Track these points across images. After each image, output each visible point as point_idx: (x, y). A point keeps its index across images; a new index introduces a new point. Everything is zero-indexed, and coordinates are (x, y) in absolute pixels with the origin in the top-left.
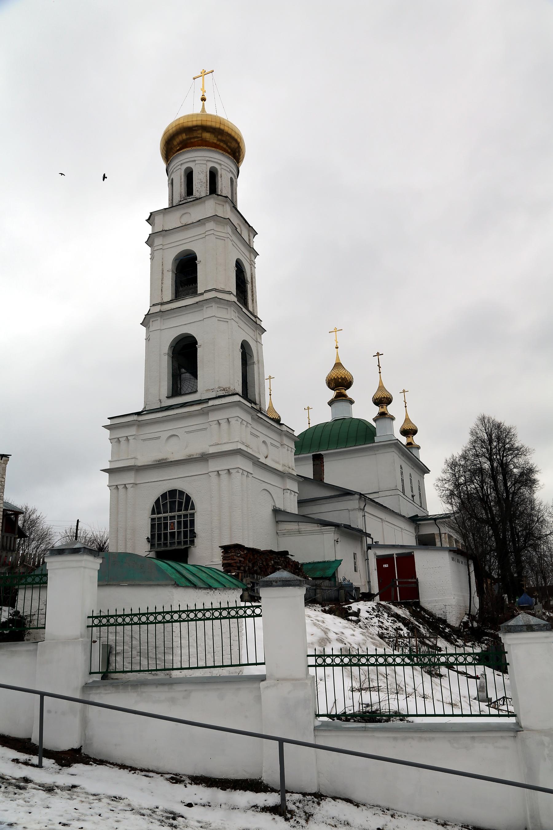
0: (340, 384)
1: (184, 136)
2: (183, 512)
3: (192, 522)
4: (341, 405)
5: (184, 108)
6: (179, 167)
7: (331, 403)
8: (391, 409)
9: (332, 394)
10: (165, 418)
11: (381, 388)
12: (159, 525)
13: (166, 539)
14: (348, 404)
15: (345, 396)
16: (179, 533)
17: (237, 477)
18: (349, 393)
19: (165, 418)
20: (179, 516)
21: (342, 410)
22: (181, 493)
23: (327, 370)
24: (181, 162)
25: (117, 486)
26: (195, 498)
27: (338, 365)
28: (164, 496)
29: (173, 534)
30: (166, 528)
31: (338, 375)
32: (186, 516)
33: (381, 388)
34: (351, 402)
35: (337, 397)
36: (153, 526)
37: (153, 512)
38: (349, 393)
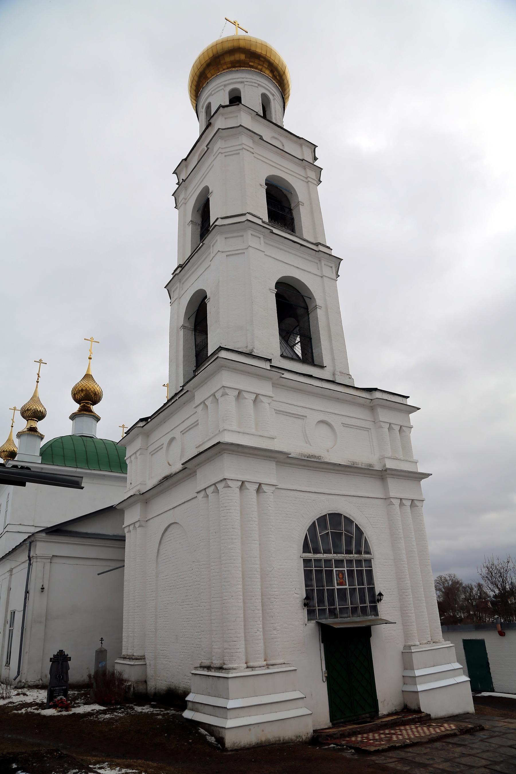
0: (87, 399)
1: (243, 57)
2: (354, 556)
3: (370, 573)
4: (86, 420)
5: (215, 33)
6: (223, 87)
7: (73, 417)
8: (40, 426)
9: (76, 407)
10: (319, 390)
11: (35, 398)
12: (319, 572)
13: (332, 602)
14: (94, 422)
15: (91, 411)
16: (353, 591)
17: (232, 495)
18: (95, 409)
19: (319, 390)
20: (350, 562)
21: (85, 426)
22: (349, 521)
23: (76, 379)
24: (260, 83)
25: (243, 482)
26: (369, 533)
27: (88, 376)
28: (322, 520)
29: (342, 593)
30: (330, 581)
31: (86, 387)
32: (359, 562)
33: (35, 398)
34: (98, 419)
35: (80, 410)
36: (308, 574)
37: (306, 548)
38: (95, 409)
